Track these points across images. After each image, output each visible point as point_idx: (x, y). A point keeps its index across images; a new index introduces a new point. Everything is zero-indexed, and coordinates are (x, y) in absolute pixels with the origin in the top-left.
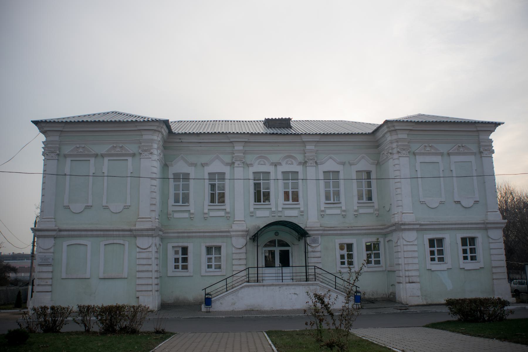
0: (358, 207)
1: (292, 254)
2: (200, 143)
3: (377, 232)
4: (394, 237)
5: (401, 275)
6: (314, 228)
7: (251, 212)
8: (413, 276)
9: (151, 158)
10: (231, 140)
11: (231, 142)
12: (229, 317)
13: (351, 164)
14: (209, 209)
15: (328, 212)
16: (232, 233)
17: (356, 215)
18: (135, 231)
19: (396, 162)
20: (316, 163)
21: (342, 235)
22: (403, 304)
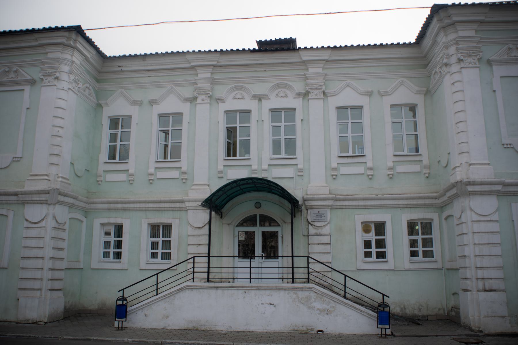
0: (393, 162)
1: (282, 238)
2: (148, 72)
3: (427, 202)
4: (455, 209)
5: (468, 277)
6: (318, 196)
7: (218, 172)
8: (491, 279)
9: (55, 85)
10: (193, 64)
11: (193, 68)
12: (139, 341)
13: (382, 95)
14: (156, 168)
15: (344, 170)
16: (187, 204)
17: (391, 176)
18: (22, 194)
19: (457, 77)
20: (324, 93)
21: (366, 207)
22: (472, 330)
